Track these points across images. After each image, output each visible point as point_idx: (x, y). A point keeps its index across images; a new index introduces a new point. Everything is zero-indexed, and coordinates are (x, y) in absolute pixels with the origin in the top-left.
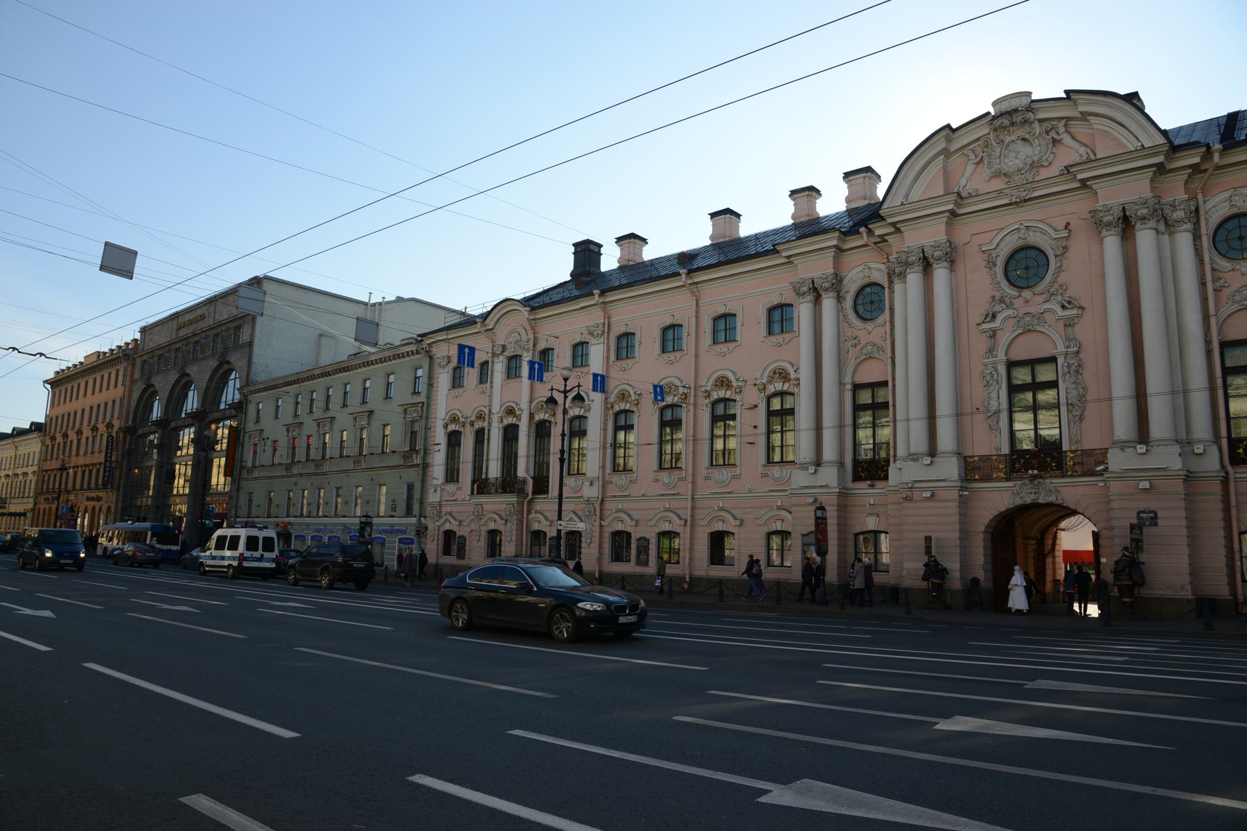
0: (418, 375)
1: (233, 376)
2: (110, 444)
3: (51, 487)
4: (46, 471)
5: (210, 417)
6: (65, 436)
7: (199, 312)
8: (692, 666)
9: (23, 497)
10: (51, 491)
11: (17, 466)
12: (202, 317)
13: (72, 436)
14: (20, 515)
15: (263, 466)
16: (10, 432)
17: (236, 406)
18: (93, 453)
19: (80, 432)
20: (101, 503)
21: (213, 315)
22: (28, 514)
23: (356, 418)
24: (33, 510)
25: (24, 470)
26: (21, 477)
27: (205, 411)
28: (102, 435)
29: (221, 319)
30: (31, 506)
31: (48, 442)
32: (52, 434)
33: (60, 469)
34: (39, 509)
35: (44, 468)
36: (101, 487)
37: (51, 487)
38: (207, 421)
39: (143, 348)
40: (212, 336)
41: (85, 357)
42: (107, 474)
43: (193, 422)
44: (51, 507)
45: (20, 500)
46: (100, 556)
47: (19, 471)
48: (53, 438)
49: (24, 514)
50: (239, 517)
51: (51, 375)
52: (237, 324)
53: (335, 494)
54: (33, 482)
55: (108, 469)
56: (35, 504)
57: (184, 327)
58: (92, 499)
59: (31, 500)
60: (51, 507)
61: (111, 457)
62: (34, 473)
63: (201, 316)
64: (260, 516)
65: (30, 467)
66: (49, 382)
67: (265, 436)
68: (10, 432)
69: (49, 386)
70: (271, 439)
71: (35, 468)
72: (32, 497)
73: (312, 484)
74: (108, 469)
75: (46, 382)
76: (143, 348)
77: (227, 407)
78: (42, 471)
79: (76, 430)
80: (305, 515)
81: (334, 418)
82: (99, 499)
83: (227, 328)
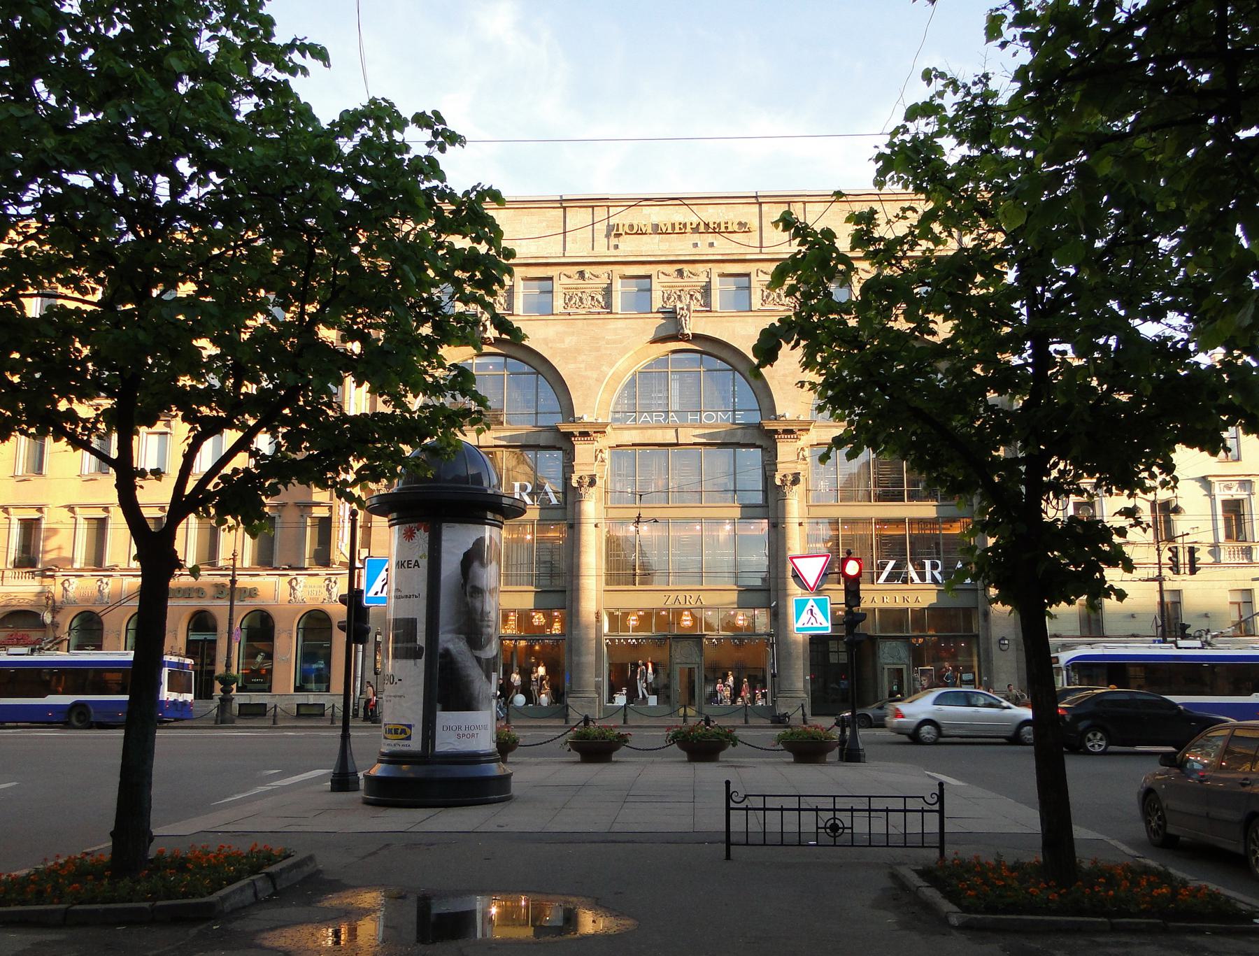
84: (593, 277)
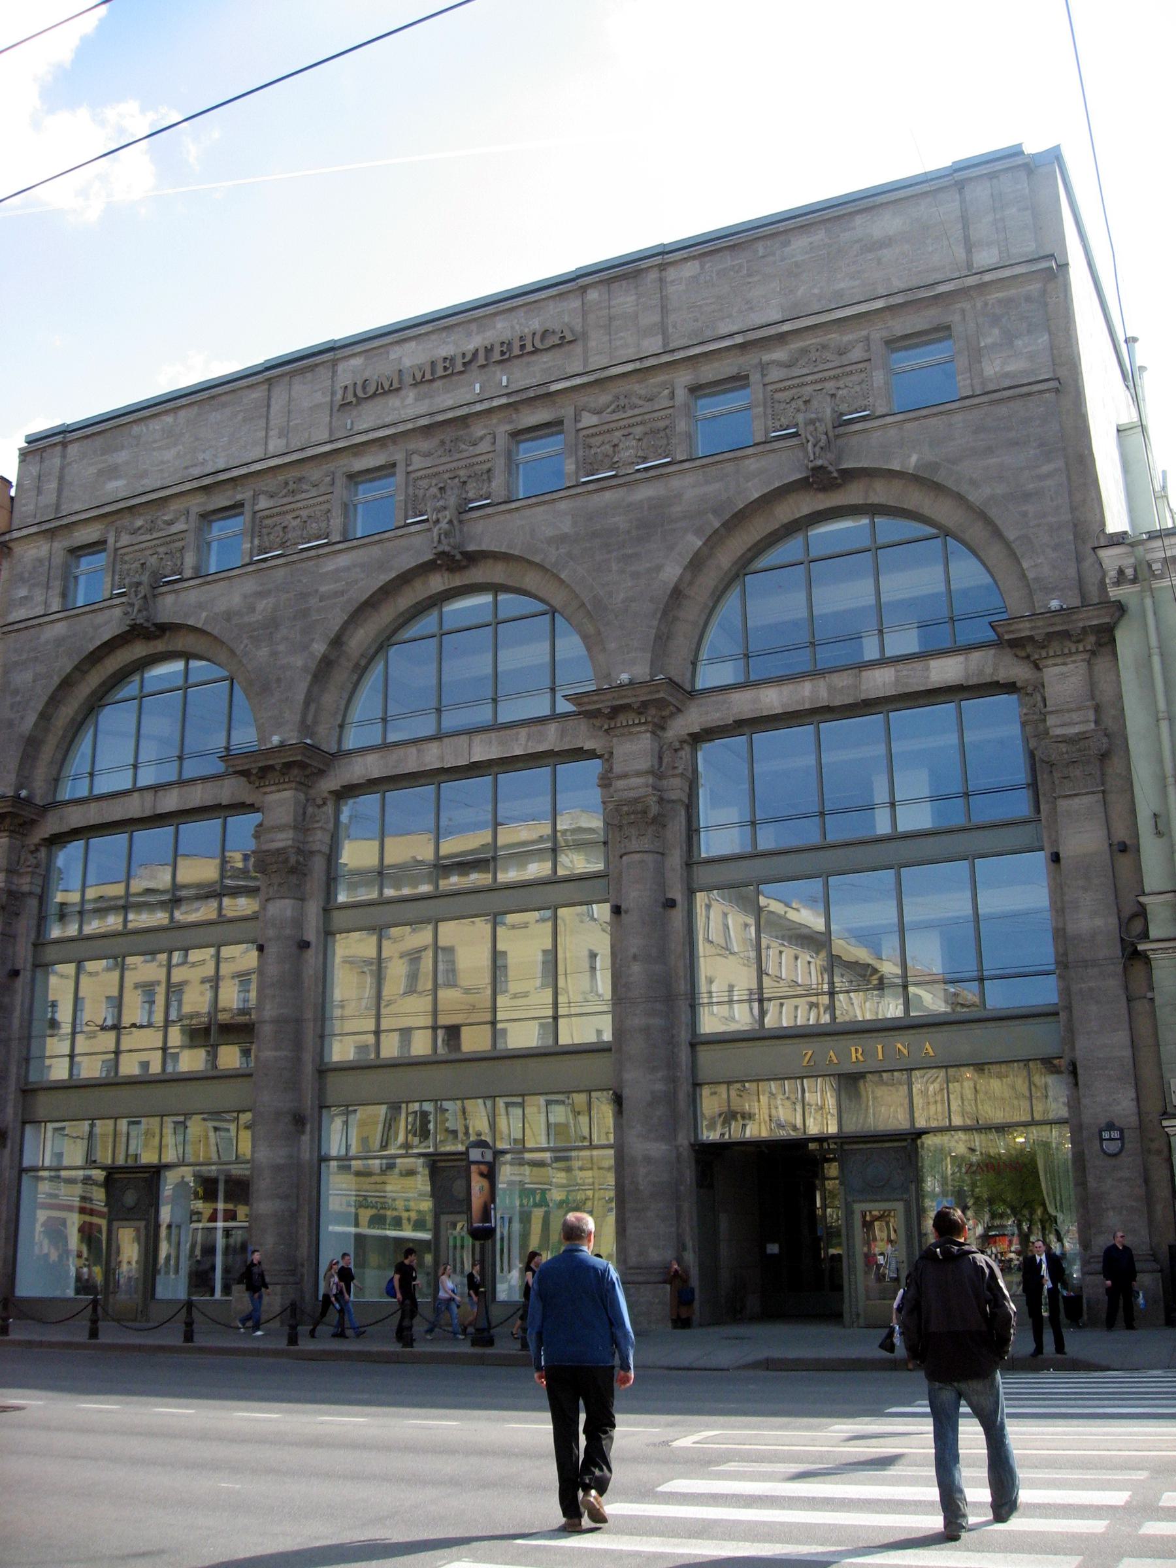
63: (545, 334)
77: (564, 707)
84: (641, 403)
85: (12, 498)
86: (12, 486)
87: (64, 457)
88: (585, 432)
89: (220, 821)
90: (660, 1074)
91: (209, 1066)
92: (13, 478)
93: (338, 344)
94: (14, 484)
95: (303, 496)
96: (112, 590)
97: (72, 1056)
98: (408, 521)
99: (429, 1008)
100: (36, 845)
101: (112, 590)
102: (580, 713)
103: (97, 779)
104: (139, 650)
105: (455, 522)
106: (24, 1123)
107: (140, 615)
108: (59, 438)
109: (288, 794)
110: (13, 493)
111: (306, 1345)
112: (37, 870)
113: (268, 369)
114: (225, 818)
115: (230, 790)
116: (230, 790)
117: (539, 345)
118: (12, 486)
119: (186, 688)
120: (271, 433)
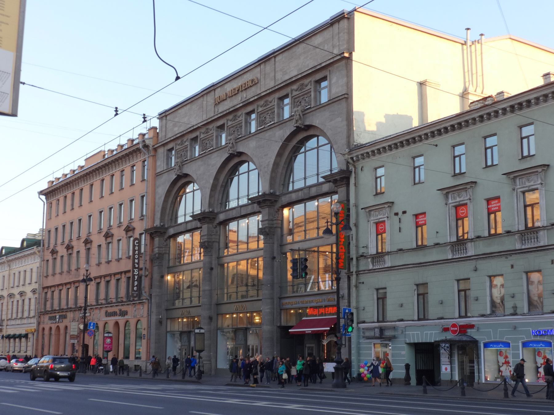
0: (378, 175)
1: (189, 189)
2: (137, 248)
3: (102, 296)
4: (47, 287)
5: (284, 200)
6: (69, 247)
7: (247, 77)
8: (52, 413)
9: (22, 318)
10: (104, 302)
11: (12, 285)
12: (254, 83)
13: (79, 246)
14: (20, 337)
15: (401, 250)
16: (18, 245)
17: (338, 178)
18: (108, 262)
19: (87, 242)
20: (126, 317)
21: (272, 74)
22: (30, 336)
23: (448, 193)
24: (37, 330)
25: (21, 289)
26: (18, 297)
27: (163, 225)
28: (62, 257)
29: (287, 77)
30: (34, 326)
31: (49, 256)
32: (52, 247)
33: (84, 281)
34: (44, 329)
35: (45, 285)
36: (124, 300)
37: (102, 296)
38: (279, 205)
39: (165, 136)
40: (276, 100)
41: (86, 160)
42: (136, 283)
43: (199, 225)
44: (58, 326)
45: (18, 322)
46: (413, 386)
47: (16, 291)
48: (54, 252)
49: (26, 336)
50: (364, 322)
51: (44, 186)
52: (318, 76)
53: (488, 284)
54: (33, 301)
55: (136, 277)
56: (39, 324)
57: (226, 99)
58: (114, 314)
59: (34, 321)
60: (58, 326)
61: (138, 264)
62: (34, 291)
63: (252, 81)
64: (405, 318)
65: (16, 288)
66: (44, 192)
67: (398, 208)
68: (18, 245)
69: (43, 197)
70: (411, 212)
71: (35, 286)
72: (34, 317)
73: (512, 266)
74: (136, 277)
75: (41, 193)
76: (165, 136)
77: (321, 180)
78: (44, 288)
79: (51, 250)
80: (359, 325)
81: (393, 203)
82: (123, 314)
83: (266, 102)
85: (158, 133)
86: (157, 129)
87: (166, 119)
88: (260, 113)
89: (237, 222)
90: (269, 307)
91: (331, 289)
92: (158, 126)
93: (215, 84)
94: (158, 127)
95: (304, 90)
96: (257, 128)
97: (191, 298)
98: (258, 129)
99: (229, 289)
100: (166, 239)
101: (257, 128)
102: (326, 182)
103: (307, 180)
104: (236, 160)
105: (234, 143)
106: (218, 315)
107: (178, 172)
108: (164, 115)
109: (343, 188)
110: (158, 131)
111: (156, 377)
112: (167, 246)
113: (202, 92)
114: (238, 221)
115: (256, 207)
116: (326, 188)
117: (219, 101)
118: (157, 129)
119: (318, 147)
120: (204, 113)
